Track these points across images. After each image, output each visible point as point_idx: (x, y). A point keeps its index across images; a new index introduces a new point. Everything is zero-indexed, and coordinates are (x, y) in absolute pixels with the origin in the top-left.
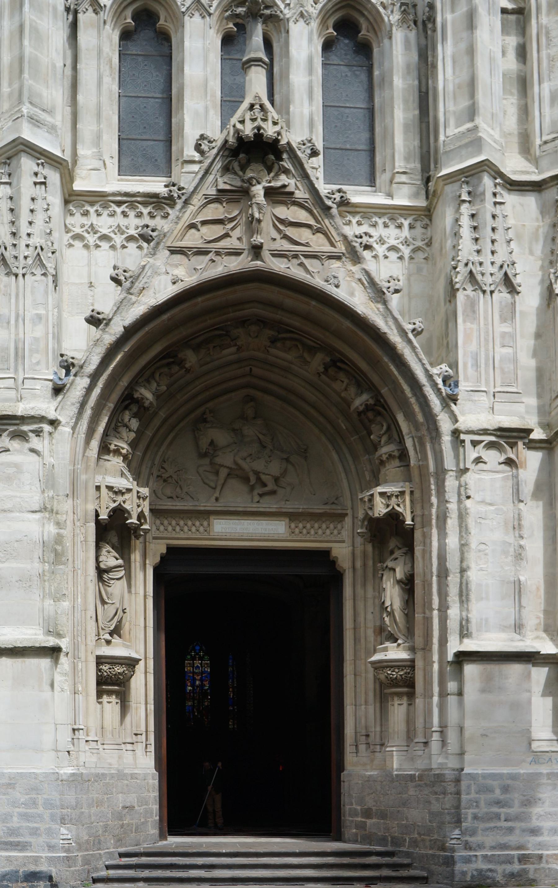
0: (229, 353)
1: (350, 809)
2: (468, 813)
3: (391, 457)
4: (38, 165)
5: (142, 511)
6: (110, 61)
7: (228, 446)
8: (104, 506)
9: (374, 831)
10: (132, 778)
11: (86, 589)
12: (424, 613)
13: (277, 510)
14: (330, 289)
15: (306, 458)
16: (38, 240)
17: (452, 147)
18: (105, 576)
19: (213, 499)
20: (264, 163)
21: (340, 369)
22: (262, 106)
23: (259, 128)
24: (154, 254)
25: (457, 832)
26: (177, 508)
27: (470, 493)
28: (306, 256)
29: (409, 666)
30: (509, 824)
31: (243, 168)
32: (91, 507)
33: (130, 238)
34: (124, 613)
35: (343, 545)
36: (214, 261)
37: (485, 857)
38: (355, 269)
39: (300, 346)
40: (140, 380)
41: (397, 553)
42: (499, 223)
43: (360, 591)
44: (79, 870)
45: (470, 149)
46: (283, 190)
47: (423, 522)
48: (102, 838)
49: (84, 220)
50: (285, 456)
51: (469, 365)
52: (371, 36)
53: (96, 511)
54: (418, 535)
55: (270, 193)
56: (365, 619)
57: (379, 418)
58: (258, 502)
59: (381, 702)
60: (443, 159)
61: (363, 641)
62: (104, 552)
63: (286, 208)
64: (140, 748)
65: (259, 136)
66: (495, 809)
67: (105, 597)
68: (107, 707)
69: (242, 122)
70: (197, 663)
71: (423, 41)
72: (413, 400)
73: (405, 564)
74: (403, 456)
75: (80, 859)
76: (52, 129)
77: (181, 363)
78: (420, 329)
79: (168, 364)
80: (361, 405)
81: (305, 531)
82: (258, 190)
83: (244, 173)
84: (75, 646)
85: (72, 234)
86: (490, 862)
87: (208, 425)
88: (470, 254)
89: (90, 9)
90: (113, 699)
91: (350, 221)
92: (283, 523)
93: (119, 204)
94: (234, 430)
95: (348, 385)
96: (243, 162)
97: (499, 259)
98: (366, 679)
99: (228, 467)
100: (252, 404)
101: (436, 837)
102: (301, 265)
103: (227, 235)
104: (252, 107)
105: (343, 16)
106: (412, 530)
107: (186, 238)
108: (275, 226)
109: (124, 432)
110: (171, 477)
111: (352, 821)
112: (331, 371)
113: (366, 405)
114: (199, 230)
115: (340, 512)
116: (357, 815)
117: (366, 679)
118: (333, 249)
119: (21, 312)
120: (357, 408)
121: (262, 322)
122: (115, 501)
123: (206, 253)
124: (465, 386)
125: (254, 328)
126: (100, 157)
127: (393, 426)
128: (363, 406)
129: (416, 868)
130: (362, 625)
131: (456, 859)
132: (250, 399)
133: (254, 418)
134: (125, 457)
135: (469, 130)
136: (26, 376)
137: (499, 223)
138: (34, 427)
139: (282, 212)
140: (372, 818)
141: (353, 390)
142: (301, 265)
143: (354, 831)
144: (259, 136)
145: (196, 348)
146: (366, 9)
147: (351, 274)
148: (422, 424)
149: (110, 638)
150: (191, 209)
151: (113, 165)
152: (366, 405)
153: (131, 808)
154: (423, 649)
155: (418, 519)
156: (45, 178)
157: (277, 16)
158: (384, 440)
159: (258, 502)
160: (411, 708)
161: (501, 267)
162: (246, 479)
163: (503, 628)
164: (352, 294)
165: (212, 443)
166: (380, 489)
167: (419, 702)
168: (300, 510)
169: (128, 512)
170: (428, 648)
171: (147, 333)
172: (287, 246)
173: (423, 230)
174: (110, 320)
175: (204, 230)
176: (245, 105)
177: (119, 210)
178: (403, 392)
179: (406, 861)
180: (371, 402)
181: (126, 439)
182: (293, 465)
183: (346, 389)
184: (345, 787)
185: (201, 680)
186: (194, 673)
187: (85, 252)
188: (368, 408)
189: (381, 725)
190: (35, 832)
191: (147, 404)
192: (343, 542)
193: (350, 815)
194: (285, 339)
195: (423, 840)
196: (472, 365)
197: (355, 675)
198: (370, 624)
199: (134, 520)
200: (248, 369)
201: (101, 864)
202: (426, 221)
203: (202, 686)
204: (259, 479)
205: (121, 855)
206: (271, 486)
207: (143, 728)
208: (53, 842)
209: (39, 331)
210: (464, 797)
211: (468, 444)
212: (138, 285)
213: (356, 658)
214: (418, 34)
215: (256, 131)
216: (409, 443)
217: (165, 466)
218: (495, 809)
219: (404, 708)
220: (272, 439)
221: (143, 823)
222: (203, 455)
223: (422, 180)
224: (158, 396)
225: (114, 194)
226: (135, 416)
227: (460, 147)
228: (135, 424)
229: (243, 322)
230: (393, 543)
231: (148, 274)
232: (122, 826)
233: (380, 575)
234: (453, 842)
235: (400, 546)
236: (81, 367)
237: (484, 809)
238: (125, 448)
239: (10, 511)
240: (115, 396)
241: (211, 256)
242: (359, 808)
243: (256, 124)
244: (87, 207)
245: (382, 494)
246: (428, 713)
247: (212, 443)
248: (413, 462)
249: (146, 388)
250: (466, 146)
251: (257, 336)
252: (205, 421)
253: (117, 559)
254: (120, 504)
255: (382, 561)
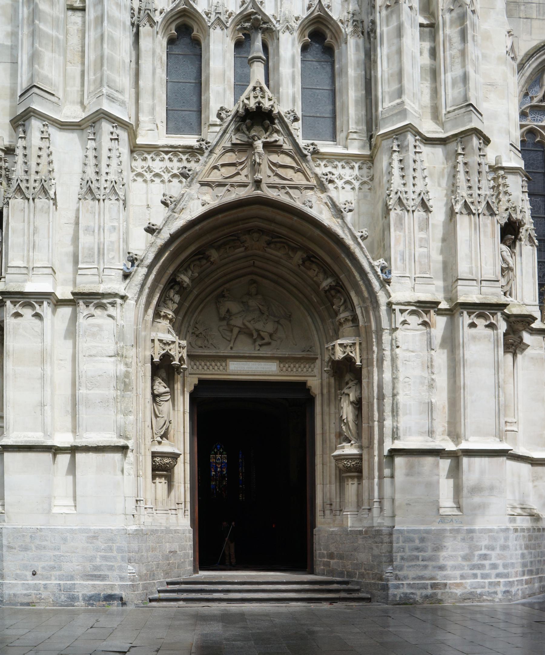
0: (240, 251)
1: (320, 553)
2: (398, 556)
3: (346, 320)
4: (113, 127)
5: (182, 356)
6: (161, 58)
7: (239, 313)
8: (157, 353)
9: (335, 567)
10: (175, 533)
11: (145, 407)
12: (369, 423)
13: (271, 355)
14: (306, 209)
15: (290, 321)
16: (113, 177)
17: (387, 115)
18: (158, 399)
19: (229, 348)
20: (263, 126)
21: (313, 262)
22: (261, 88)
23: (259, 103)
24: (190, 186)
25: (390, 568)
26: (205, 354)
27: (399, 344)
28: (290, 188)
29: (358, 459)
30: (425, 563)
31: (249, 129)
32: (148, 353)
33: (174, 176)
34: (170, 423)
35: (315, 378)
36: (229, 191)
37: (409, 584)
38: (323, 196)
39: (286, 247)
40: (181, 270)
41: (351, 384)
42: (418, 166)
43: (326, 409)
44: (140, 594)
45: (399, 117)
46: (275, 144)
47: (368, 363)
48: (156, 572)
49: (143, 164)
50: (277, 320)
51: (398, 259)
52: (333, 42)
53: (152, 356)
54: (364, 372)
55: (267, 146)
56: (329, 427)
57: (338, 295)
58: (259, 350)
59: (340, 482)
60: (381, 123)
61: (328, 442)
62: (157, 383)
63: (277, 156)
64: (180, 513)
65: (259, 108)
66: (416, 553)
67: (157, 413)
68: (159, 486)
69: (248, 99)
70: (218, 456)
71: (368, 46)
72: (361, 283)
73: (356, 391)
74: (355, 319)
75: (141, 586)
76: (123, 103)
77: (208, 258)
78: (366, 236)
79: (199, 259)
80: (327, 286)
81: (289, 369)
82: (259, 144)
83: (249, 132)
84: (138, 445)
85: (153, 173)
86: (412, 588)
87: (225, 299)
88: (399, 186)
89: (148, 24)
90: (163, 480)
91: (319, 164)
92: (275, 364)
93: (167, 153)
94: (243, 302)
95: (318, 272)
96: (249, 125)
97: (418, 189)
98: (330, 467)
99: (239, 327)
100: (255, 285)
101: (376, 571)
102: (287, 193)
103: (238, 174)
104: (254, 89)
105: (314, 29)
106: (361, 369)
107: (211, 175)
108: (270, 167)
109: (170, 304)
110: (201, 333)
111: (321, 561)
112: (307, 263)
113: (330, 286)
114: (219, 170)
115: (313, 356)
116: (324, 557)
117: (330, 467)
118: (308, 183)
119: (102, 224)
120: (324, 288)
121: (261, 231)
122: (164, 350)
123: (224, 185)
124: (395, 273)
125: (256, 235)
126: (154, 122)
127: (348, 300)
128: (328, 287)
129: (363, 592)
130: (328, 431)
131: (390, 586)
132: (254, 282)
133: (256, 294)
134: (171, 321)
135: (398, 104)
136: (105, 267)
137: (418, 166)
138: (110, 300)
139: (274, 158)
140: (334, 559)
141: (321, 276)
142: (287, 193)
143: (322, 567)
144: (259, 108)
145: (218, 249)
146: (330, 24)
147: (320, 199)
148: (367, 298)
149: (161, 440)
150: (214, 156)
151: (163, 127)
152: (330, 286)
153: (175, 552)
154: (368, 447)
155: (364, 362)
156: (118, 136)
157: (271, 29)
158: (342, 309)
159: (259, 350)
160: (360, 486)
161: (420, 194)
162: (251, 335)
163: (421, 433)
164: (321, 213)
165: (228, 311)
166: (339, 341)
167: (365, 482)
168: (287, 356)
169: (173, 357)
170: (371, 447)
171: (185, 238)
172: (278, 180)
173: (368, 170)
174: (161, 230)
175: (223, 170)
176: (250, 87)
177: (167, 157)
178: (354, 277)
179: (357, 587)
180: (334, 284)
181: (171, 308)
182: (282, 325)
183: (317, 276)
184: (316, 538)
185: (221, 468)
186: (216, 463)
187: (144, 185)
188: (331, 288)
189: (340, 498)
190: (111, 568)
191: (185, 285)
192: (315, 376)
193: (319, 557)
194: (276, 242)
195: (368, 573)
196: (400, 260)
197: (323, 464)
198: (333, 431)
199: (176, 362)
200: (252, 262)
201: (155, 590)
202: (370, 164)
203: (222, 471)
204: (259, 335)
205: (168, 583)
206: (267, 340)
207: (182, 500)
208: (124, 574)
209: (114, 237)
210: (395, 545)
211: (397, 312)
212: (180, 207)
213: (323, 453)
214: (364, 40)
215: (257, 105)
216: (358, 311)
217: (197, 326)
218: (416, 553)
219: (355, 486)
220: (268, 308)
221: (182, 562)
222: (222, 319)
223: (367, 137)
224: (192, 280)
225: (163, 147)
226: (177, 293)
227: (392, 115)
228: (177, 298)
229: (249, 231)
230: (348, 377)
231: (186, 199)
232: (169, 564)
233: (339, 399)
234: (388, 575)
235: (352, 379)
236: (142, 261)
237: (408, 553)
238: (171, 314)
239: (95, 356)
240: (164, 280)
241: (228, 187)
242: (325, 552)
243: (257, 100)
244: (146, 155)
245: (341, 345)
246: (371, 490)
247: (228, 311)
248: (361, 323)
249: (184, 275)
250: (396, 114)
251: (258, 241)
252: (224, 296)
253: (165, 388)
254: (167, 351)
255: (341, 389)
